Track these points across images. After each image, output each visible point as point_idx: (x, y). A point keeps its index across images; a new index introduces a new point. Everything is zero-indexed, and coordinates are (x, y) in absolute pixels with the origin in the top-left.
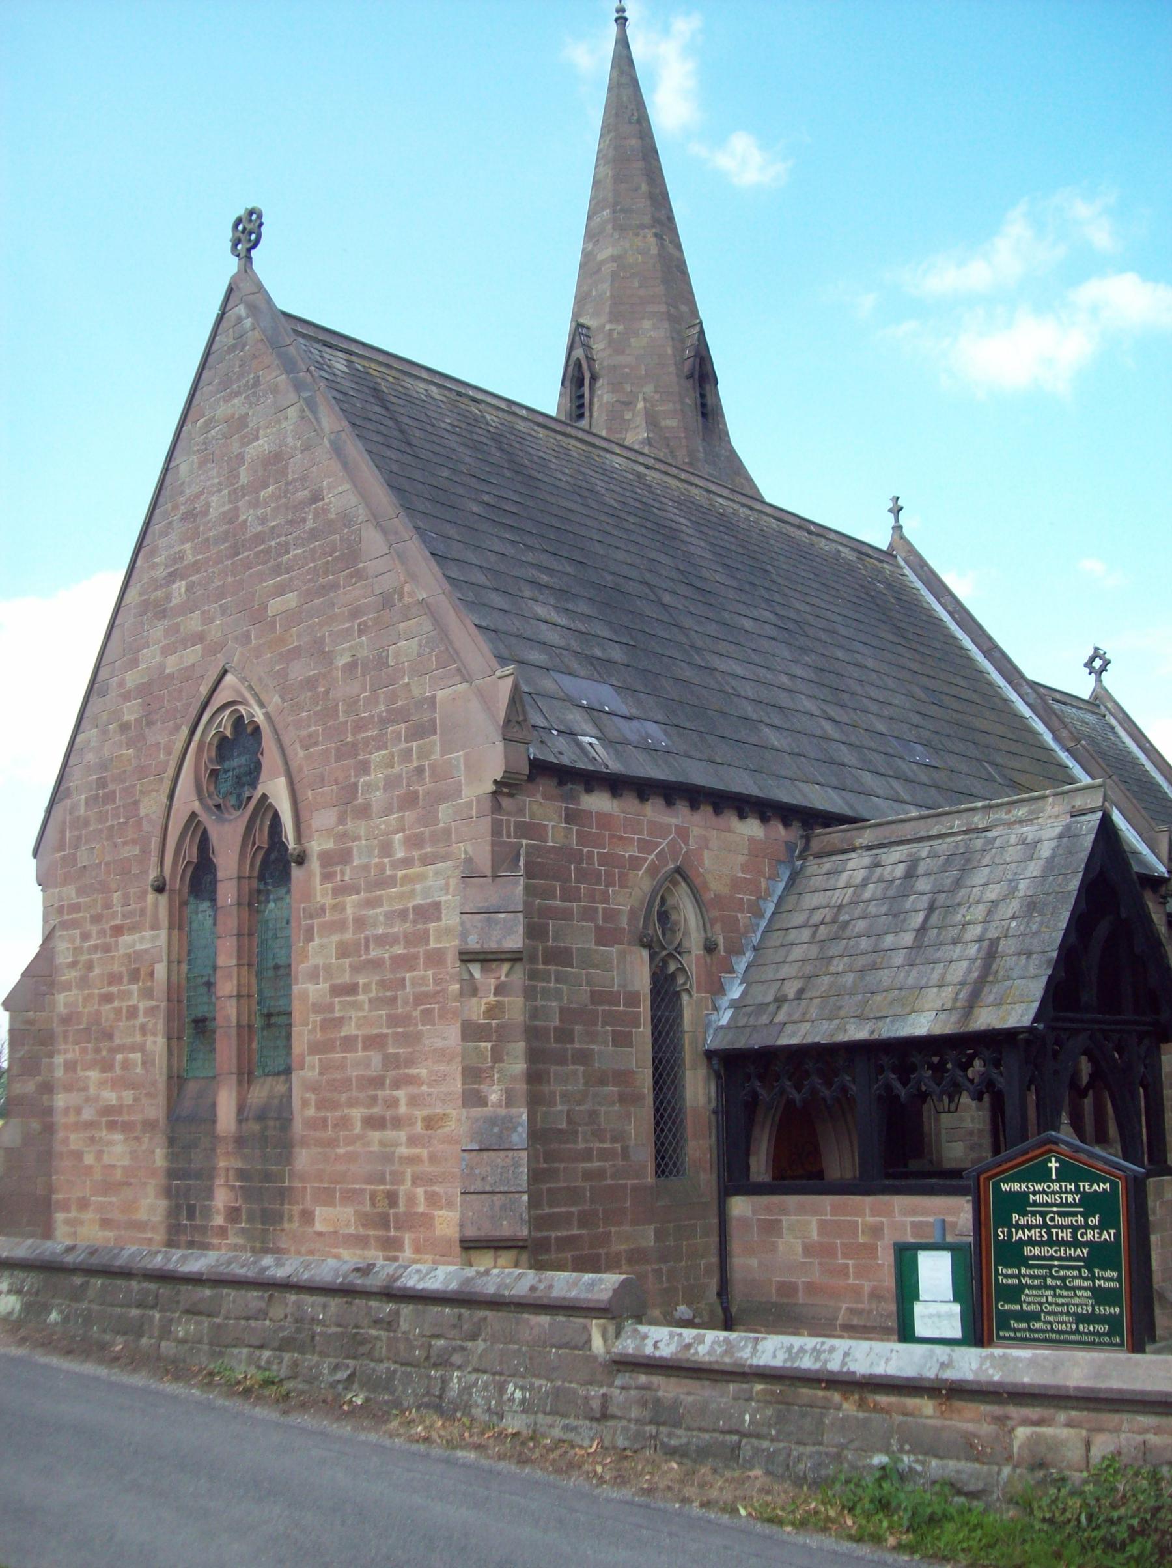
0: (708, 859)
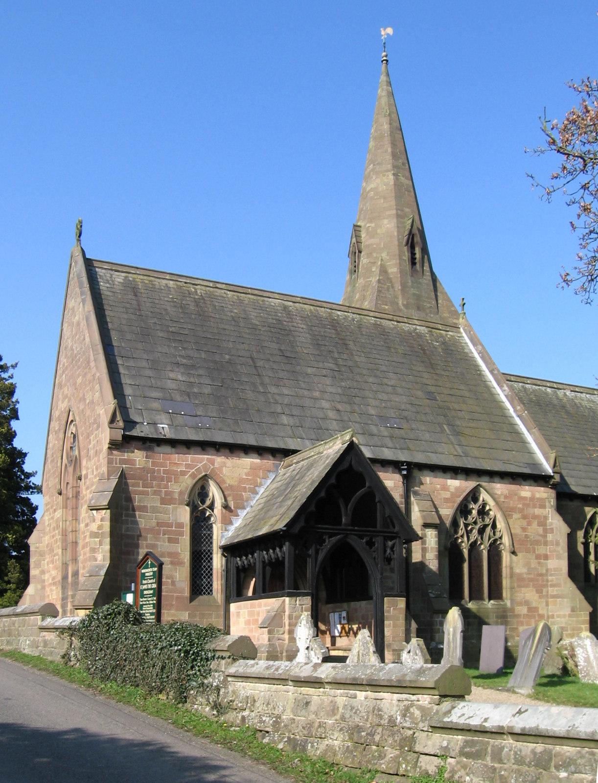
0: (225, 470)
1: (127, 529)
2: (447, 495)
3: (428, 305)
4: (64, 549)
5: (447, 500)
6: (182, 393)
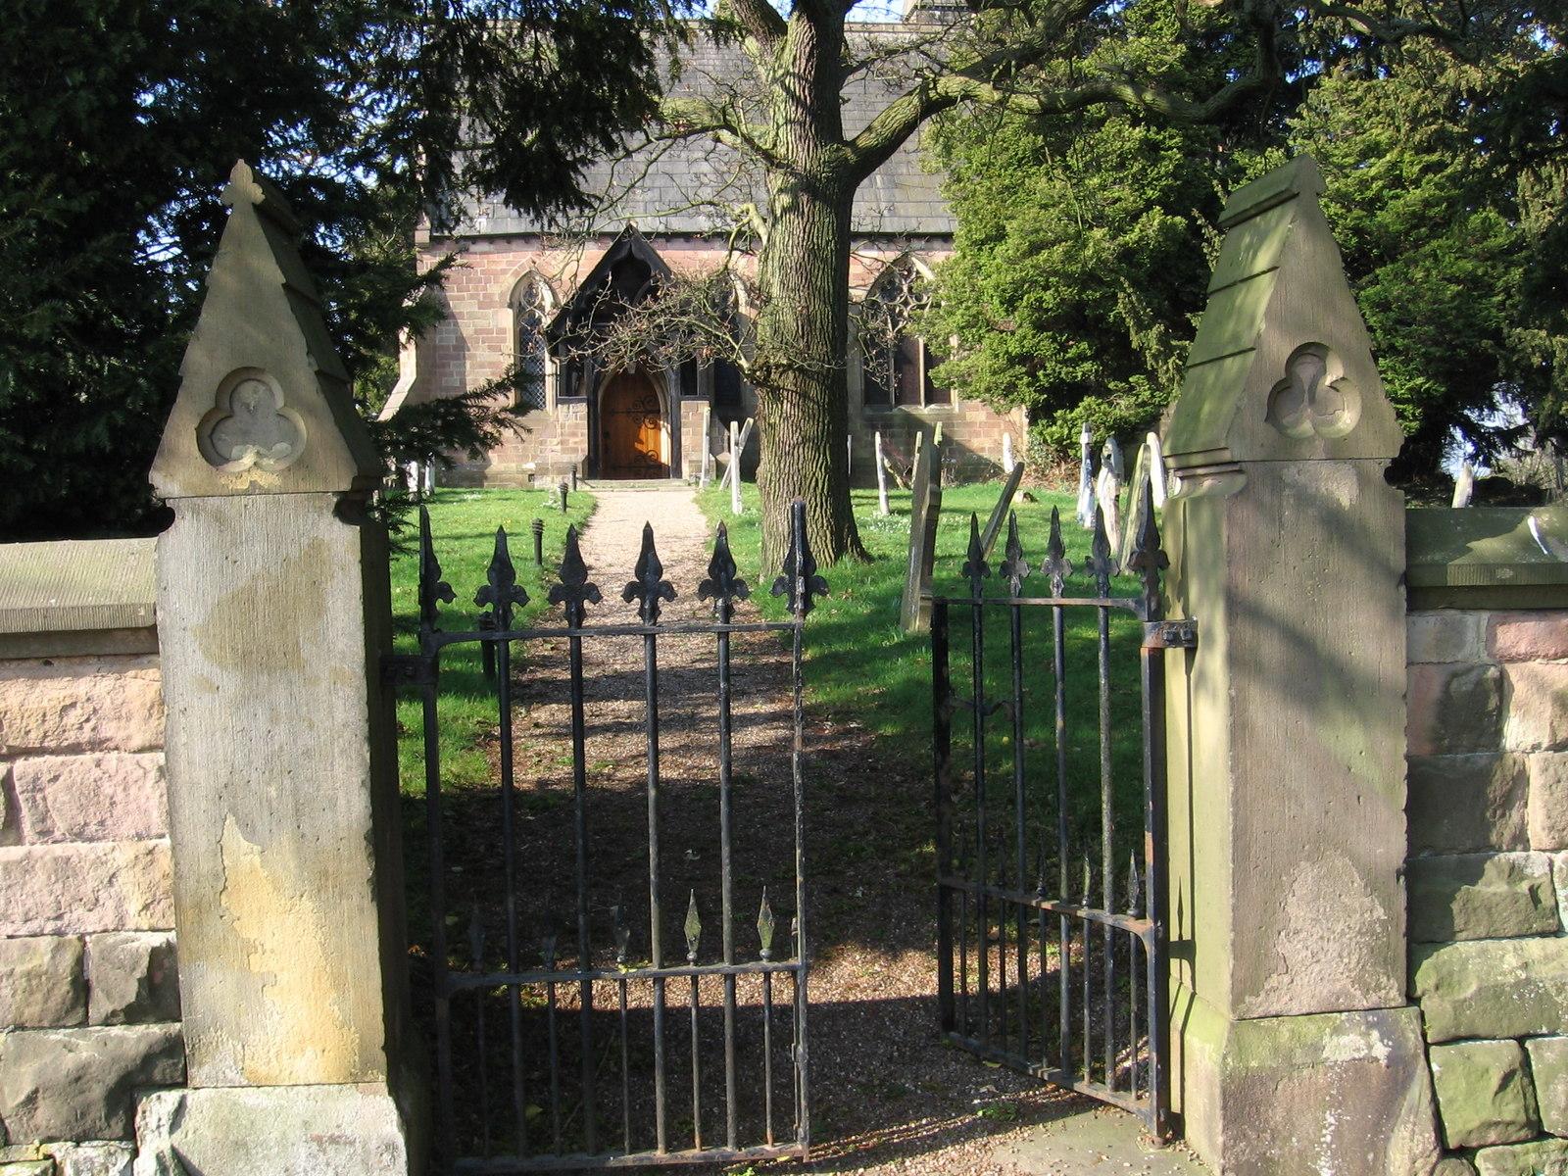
1: (441, 340)
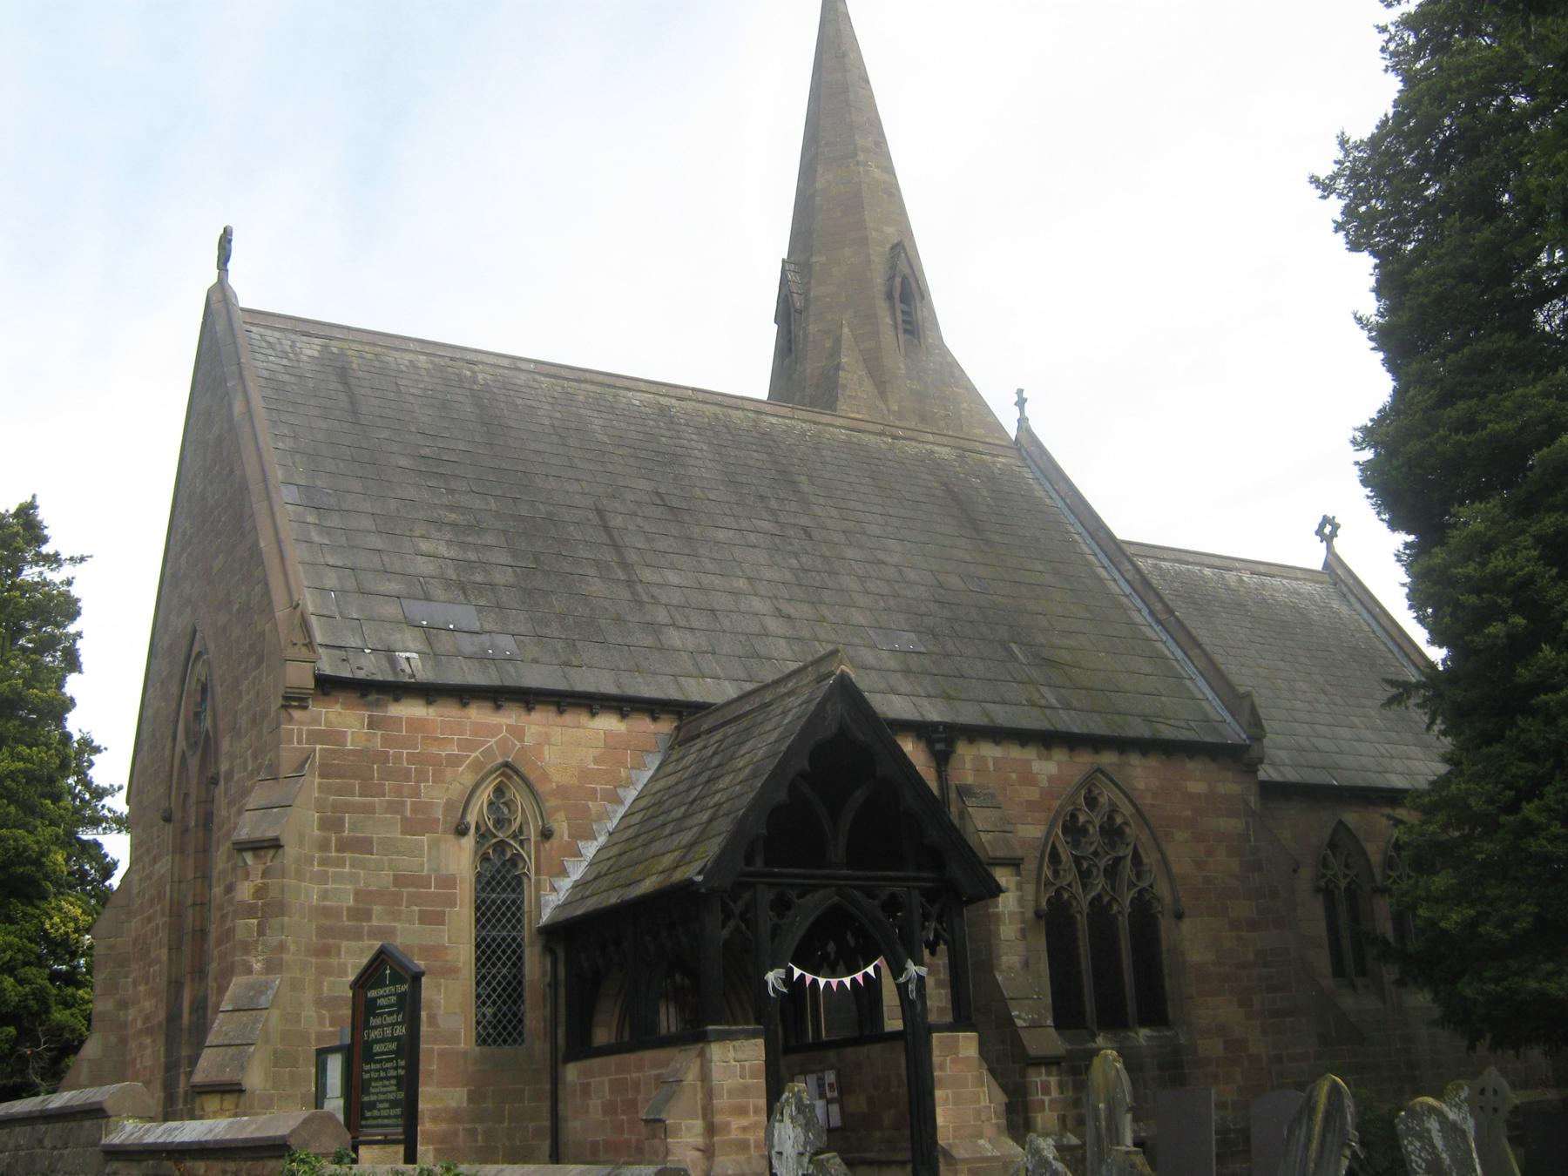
2: (1033, 794)
3: (942, 413)
4: (175, 947)
5: (1032, 806)
6: (448, 584)
